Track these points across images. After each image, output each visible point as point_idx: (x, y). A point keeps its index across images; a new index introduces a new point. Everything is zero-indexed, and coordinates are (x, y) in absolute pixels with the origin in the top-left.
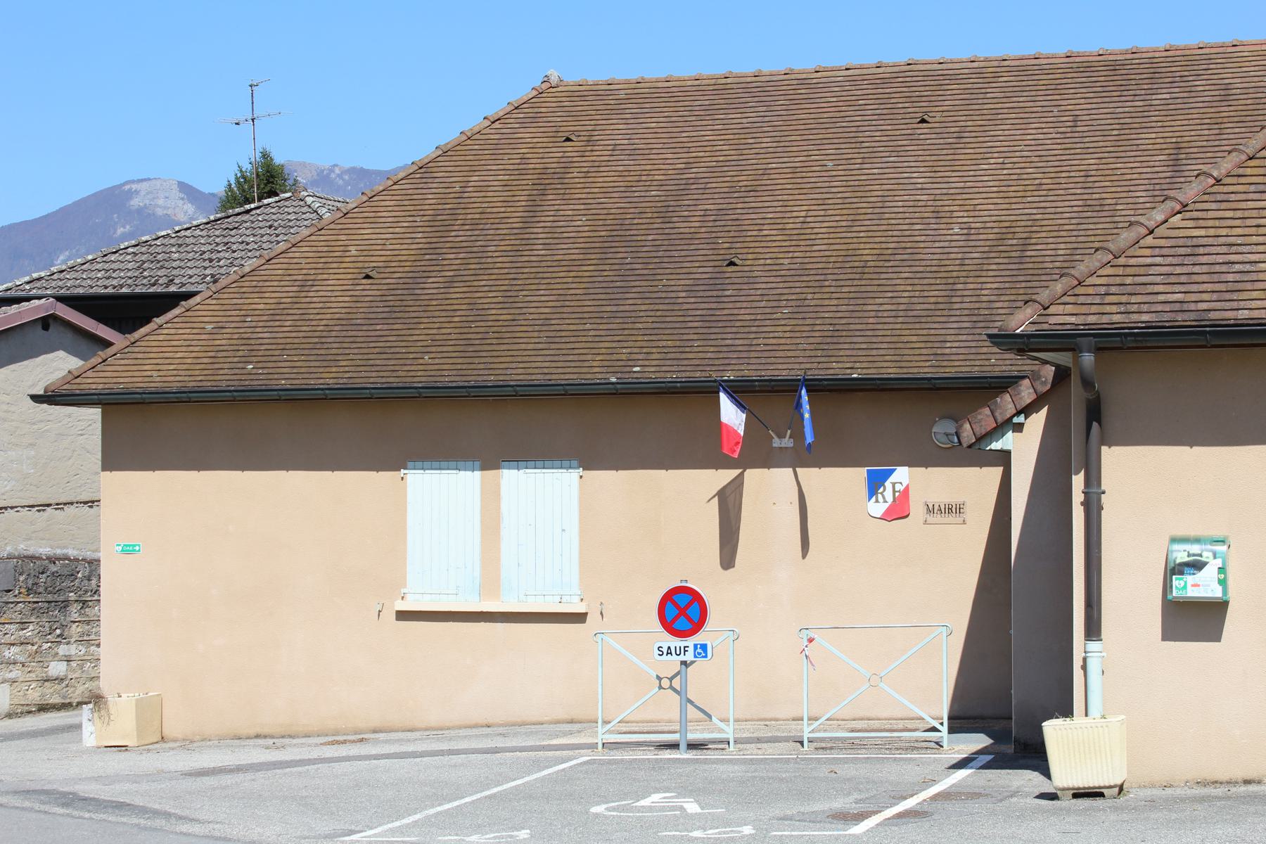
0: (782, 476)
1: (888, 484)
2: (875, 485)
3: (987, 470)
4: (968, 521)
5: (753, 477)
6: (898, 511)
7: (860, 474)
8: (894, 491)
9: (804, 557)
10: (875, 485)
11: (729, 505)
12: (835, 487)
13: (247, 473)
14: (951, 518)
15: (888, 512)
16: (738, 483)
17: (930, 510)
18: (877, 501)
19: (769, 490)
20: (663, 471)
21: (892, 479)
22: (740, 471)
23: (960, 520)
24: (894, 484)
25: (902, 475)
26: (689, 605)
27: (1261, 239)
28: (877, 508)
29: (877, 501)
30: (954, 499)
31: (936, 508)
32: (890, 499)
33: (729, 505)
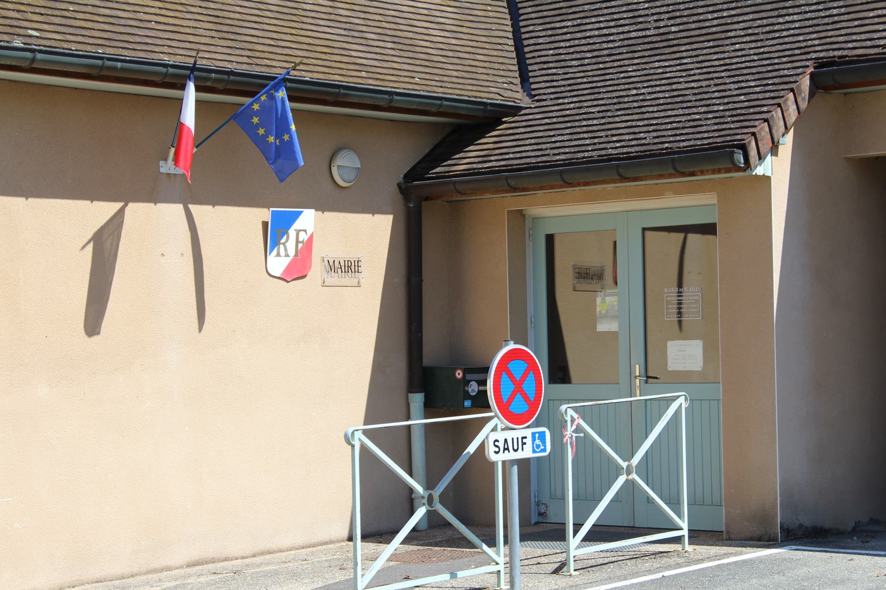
0: (171, 213)
1: (292, 232)
2: (273, 233)
3: (379, 218)
4: (363, 282)
5: (138, 213)
6: (297, 271)
7: (257, 216)
8: (297, 242)
9: (200, 330)
10: (273, 233)
11: (105, 246)
12: (231, 228)
13: (220, 209)
14: (349, 279)
15: (289, 269)
16: (116, 223)
17: (332, 267)
18: (278, 255)
19: (155, 228)
20: (22, 200)
21: (298, 225)
22: (122, 204)
23: (354, 282)
24: (298, 232)
25: (308, 220)
26: (525, 376)
27: (881, 27)
28: (278, 264)
29: (278, 255)
30: (352, 256)
31: (337, 264)
32: (292, 252)
33: (105, 246)
